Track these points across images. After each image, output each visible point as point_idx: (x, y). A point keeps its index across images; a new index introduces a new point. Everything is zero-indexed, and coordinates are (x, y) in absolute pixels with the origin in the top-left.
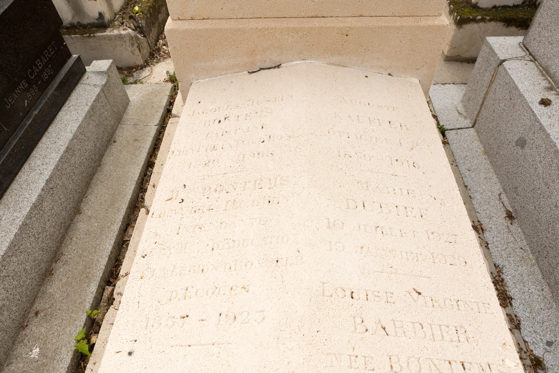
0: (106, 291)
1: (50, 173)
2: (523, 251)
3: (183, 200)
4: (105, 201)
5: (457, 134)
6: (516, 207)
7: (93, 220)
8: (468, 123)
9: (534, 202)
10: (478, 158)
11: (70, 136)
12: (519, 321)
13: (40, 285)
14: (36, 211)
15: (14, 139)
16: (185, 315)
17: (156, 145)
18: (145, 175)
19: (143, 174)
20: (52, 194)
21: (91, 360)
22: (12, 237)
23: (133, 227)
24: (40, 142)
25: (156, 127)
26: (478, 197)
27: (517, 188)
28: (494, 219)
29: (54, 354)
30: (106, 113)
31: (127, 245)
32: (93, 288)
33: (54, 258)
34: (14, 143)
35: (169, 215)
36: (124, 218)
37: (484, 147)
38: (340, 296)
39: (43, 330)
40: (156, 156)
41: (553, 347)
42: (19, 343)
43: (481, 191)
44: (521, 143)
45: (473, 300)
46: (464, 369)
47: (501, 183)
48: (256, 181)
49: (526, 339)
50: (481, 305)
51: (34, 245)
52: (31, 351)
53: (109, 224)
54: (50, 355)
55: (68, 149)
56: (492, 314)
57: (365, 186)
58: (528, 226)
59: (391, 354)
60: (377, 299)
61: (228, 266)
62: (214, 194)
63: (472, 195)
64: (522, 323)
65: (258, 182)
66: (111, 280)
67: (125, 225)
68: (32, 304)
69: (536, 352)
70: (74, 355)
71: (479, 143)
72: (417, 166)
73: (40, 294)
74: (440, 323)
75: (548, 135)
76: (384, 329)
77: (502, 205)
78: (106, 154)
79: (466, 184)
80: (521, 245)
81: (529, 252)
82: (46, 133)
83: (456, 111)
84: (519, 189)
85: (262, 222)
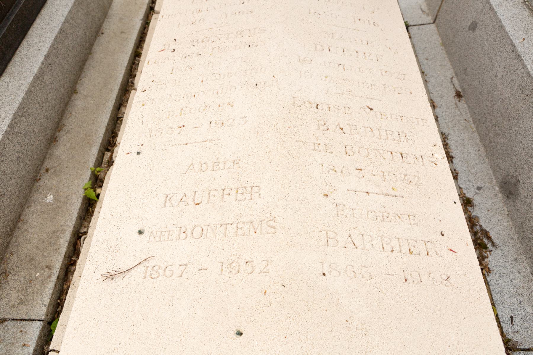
0: (105, 155)
1: (47, 49)
2: (466, 122)
3: (174, 50)
4: (99, 83)
5: (419, 29)
6: (464, 87)
7: (89, 99)
8: (430, 19)
9: (479, 78)
10: (436, 49)
11: (62, 19)
12: (457, 174)
13: (47, 149)
14: (39, 82)
15: (11, 15)
16: (182, 125)
17: (141, 38)
18: (134, 63)
19: (131, 62)
20: (51, 70)
21: (98, 205)
22: (20, 100)
23: (126, 106)
24: (34, 23)
25: (141, 22)
26: (433, 81)
27: (466, 69)
28: (445, 98)
29: (66, 200)
30: (93, 4)
31: (121, 121)
32: (95, 151)
33: (57, 127)
34: (12, 19)
35: (163, 61)
36: (117, 97)
37: (442, 39)
38: (308, 106)
39: (54, 182)
40: (142, 48)
41: (482, 190)
42: (35, 191)
43: (436, 76)
44: (473, 27)
45: (414, 117)
46: (402, 157)
47: (454, 68)
48: (237, 32)
49: (461, 186)
50: (420, 120)
51: (39, 111)
52: (46, 197)
53: (104, 102)
54: (62, 200)
55: (61, 31)
56: (429, 126)
57: (331, 36)
58: (472, 100)
59: (346, 144)
60: (337, 110)
61: (215, 91)
62: (202, 44)
63: (428, 80)
64: (459, 175)
65: (239, 33)
66: (109, 148)
67: (118, 104)
68: (43, 162)
69: (468, 195)
70: (83, 201)
71: (438, 36)
72: (376, 25)
73: (48, 156)
74: (387, 129)
75: (496, 13)
76: (342, 129)
77: (453, 86)
78: (95, 44)
79: (423, 71)
80: (465, 117)
81: (472, 122)
82: (39, 16)
83: (420, 10)
84: (468, 70)
85: (243, 60)
